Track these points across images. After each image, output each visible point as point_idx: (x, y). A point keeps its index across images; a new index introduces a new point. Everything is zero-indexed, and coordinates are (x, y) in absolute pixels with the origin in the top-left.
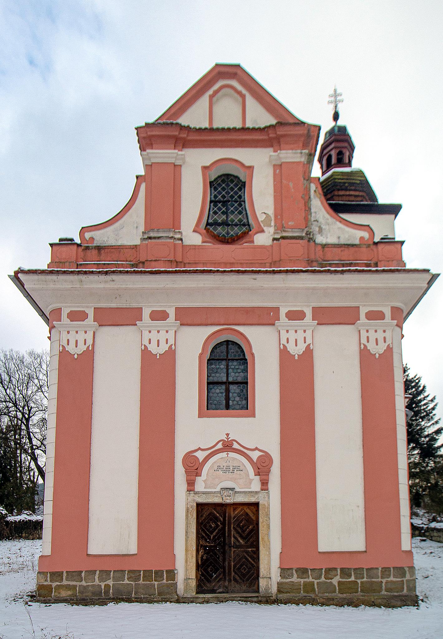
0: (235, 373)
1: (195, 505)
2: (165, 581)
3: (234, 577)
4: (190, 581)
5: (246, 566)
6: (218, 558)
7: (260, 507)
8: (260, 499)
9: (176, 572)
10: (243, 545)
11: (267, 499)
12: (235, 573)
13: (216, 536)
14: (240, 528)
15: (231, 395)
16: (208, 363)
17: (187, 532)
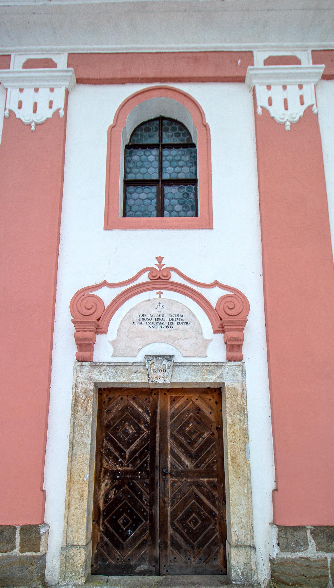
0: (174, 167)
1: (92, 387)
2: (17, 551)
3: (171, 536)
4: (73, 551)
5: (199, 514)
6: (141, 497)
7: (227, 395)
8: (228, 377)
9: (42, 531)
10: (190, 471)
11: (239, 378)
12: (176, 530)
13: (135, 451)
14: (184, 435)
15: (166, 201)
16: (125, 152)
17: (72, 444)
